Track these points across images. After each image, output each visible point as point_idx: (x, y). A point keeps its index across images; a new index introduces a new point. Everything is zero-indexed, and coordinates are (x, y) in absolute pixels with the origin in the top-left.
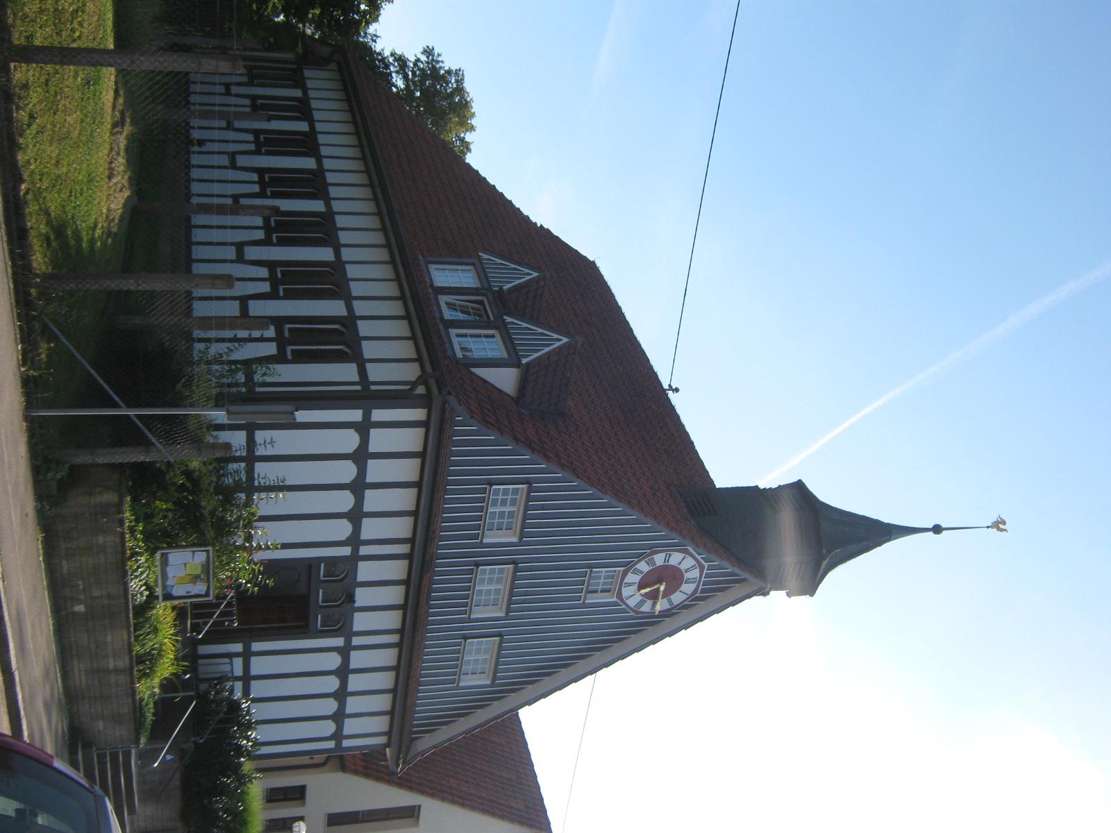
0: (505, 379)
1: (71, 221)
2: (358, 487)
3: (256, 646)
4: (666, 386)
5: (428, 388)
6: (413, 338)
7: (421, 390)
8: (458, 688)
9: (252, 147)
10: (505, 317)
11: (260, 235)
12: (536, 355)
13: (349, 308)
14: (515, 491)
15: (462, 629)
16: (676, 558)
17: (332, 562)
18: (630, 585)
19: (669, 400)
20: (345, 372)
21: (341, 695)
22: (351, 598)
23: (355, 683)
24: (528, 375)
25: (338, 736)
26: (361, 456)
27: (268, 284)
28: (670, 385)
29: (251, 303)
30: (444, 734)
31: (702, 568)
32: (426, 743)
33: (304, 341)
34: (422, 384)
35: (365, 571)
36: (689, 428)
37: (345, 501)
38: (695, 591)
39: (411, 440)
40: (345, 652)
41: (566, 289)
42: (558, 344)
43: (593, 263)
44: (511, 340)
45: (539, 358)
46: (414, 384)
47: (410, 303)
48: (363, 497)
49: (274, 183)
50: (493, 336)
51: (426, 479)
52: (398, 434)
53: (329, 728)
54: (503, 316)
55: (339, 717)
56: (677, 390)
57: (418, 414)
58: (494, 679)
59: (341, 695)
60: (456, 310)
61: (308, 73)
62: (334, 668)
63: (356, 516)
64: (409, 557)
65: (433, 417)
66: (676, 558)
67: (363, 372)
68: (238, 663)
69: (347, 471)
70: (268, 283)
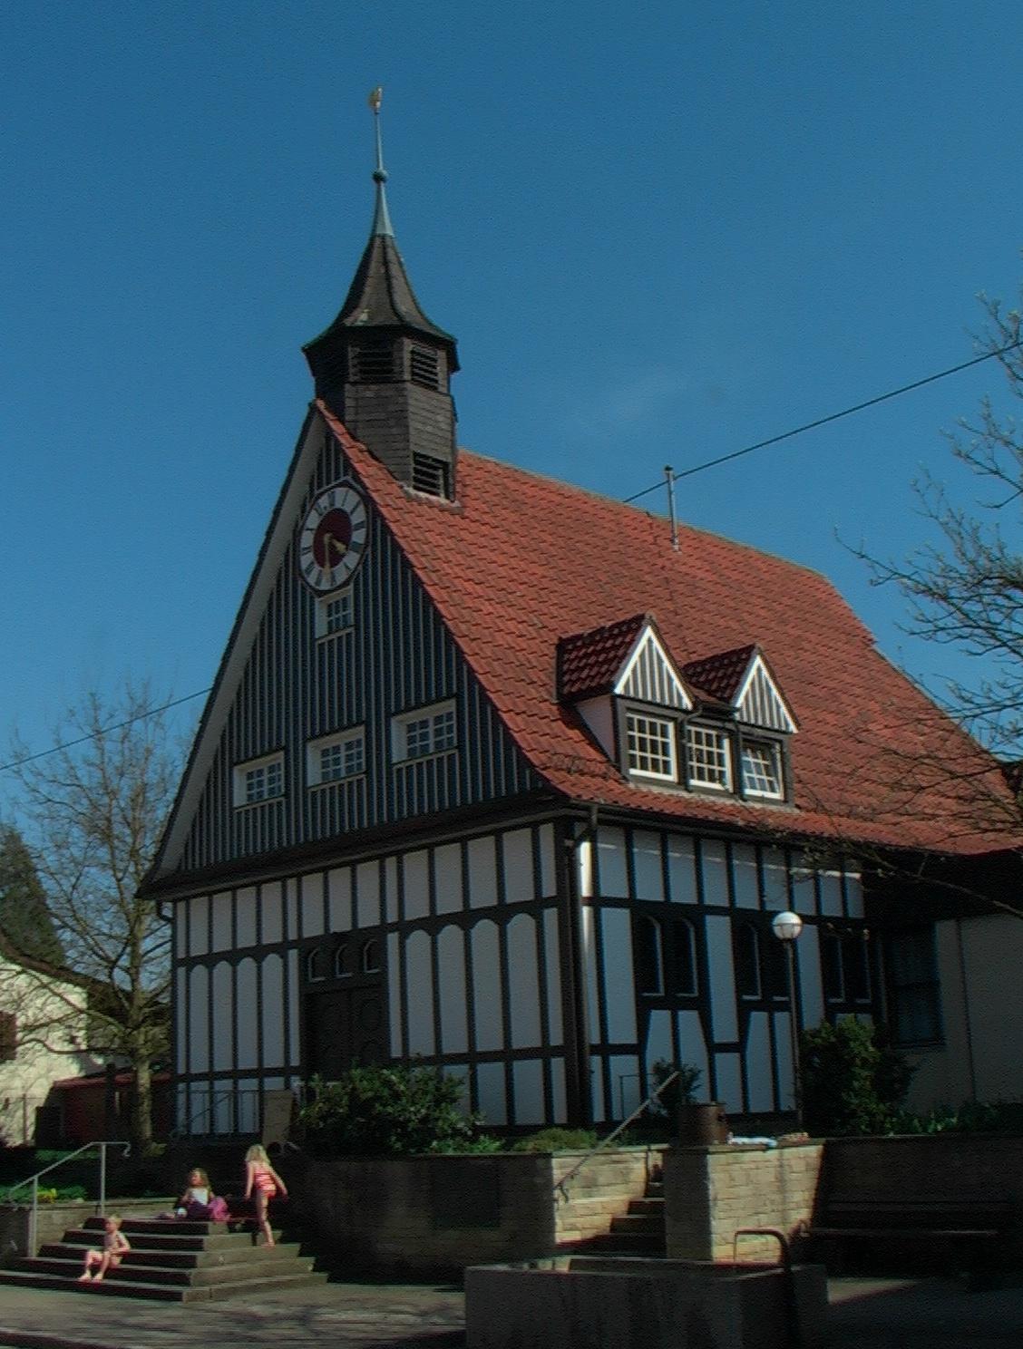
1: (329, 1121)
8: (389, 716)
35: (649, 891)
40: (405, 928)
48: (514, 904)
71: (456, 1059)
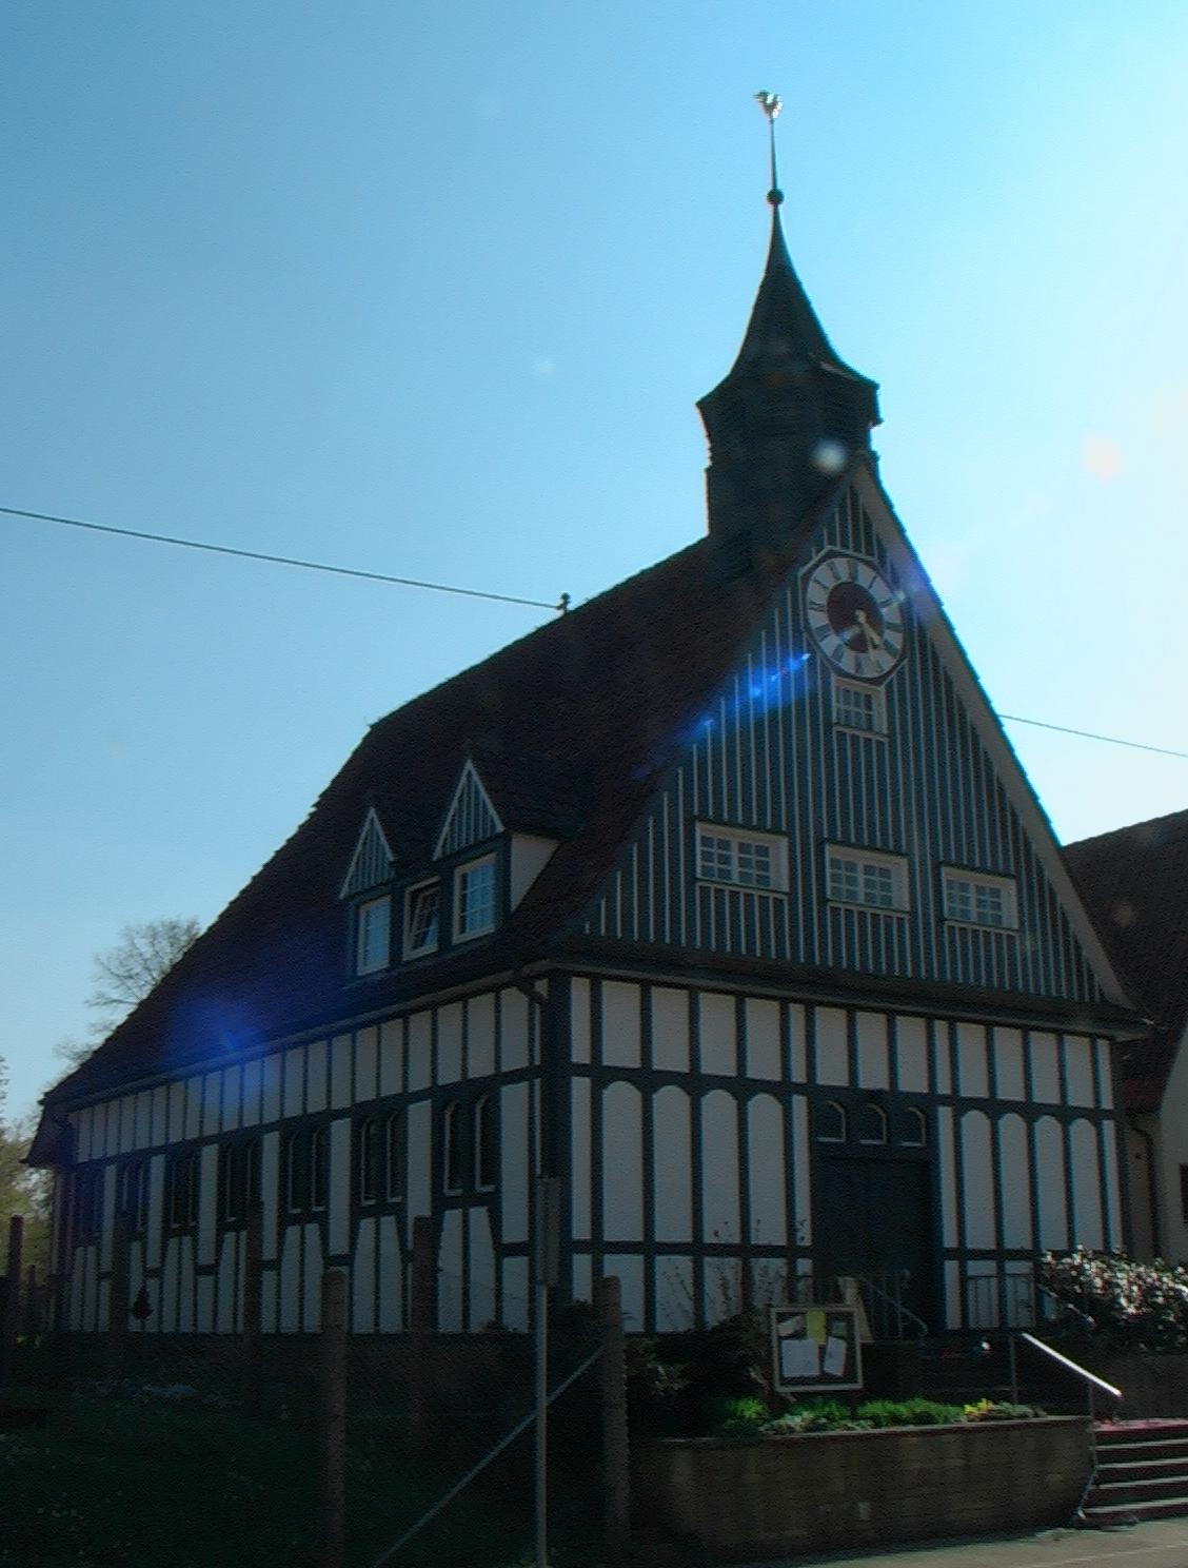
0: (529, 857)
2: (695, 1083)
3: (950, 1240)
4: (559, 614)
5: (539, 976)
6: (463, 998)
7: (541, 987)
9: (187, 1240)
10: (435, 859)
11: (479, 1215)
12: (492, 811)
13: (419, 1096)
14: (706, 841)
15: (927, 924)
16: (817, 594)
17: (816, 1125)
18: (858, 666)
19: (580, 608)
20: (515, 1103)
21: (1029, 1111)
22: (874, 1095)
23: (1046, 1093)
24: (516, 824)
25: (1095, 1116)
26: (647, 1079)
27: (309, 1226)
28: (559, 608)
29: (506, 1239)
30: (1094, 952)
31: (832, 555)
32: (1107, 980)
33: (468, 1167)
34: (533, 986)
35: (832, 1073)
36: (620, 578)
37: (718, 1104)
38: (868, 563)
39: (621, 1001)
40: (961, 1105)
41: (405, 763)
42: (476, 777)
43: (373, 727)
44: (470, 848)
45: (496, 805)
46: (534, 998)
47: (413, 1003)
49: (239, 1207)
50: (464, 877)
51: (774, 992)
52: (614, 1020)
53: (1081, 1129)
54: (433, 862)
55: (1065, 1114)
56: (565, 597)
57: (579, 990)
58: (1007, 875)
59: (1029, 1111)
60: (426, 933)
61: (83, 1158)
62: (988, 1122)
63: (742, 1088)
64: (952, 1022)
65: (799, 995)
66: (817, 594)
67: (514, 1077)
68: (975, 1267)
69: (718, 1104)
70: (472, 1210)
71: (770, 1251)
